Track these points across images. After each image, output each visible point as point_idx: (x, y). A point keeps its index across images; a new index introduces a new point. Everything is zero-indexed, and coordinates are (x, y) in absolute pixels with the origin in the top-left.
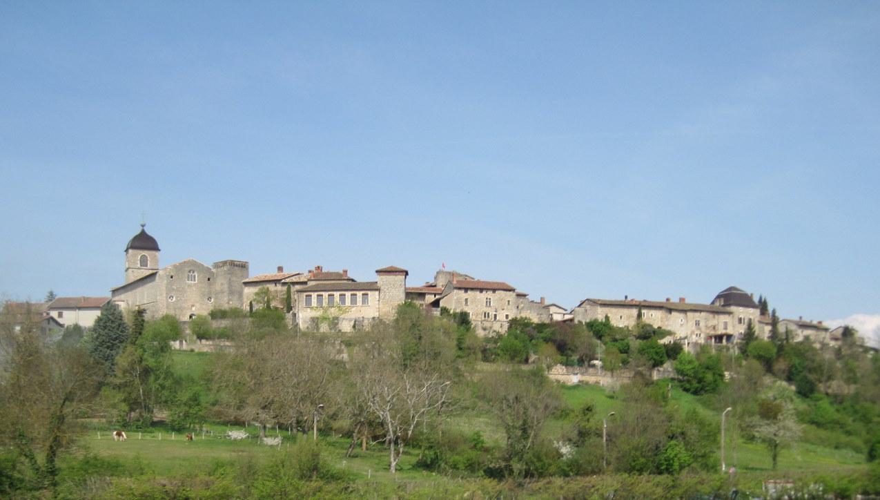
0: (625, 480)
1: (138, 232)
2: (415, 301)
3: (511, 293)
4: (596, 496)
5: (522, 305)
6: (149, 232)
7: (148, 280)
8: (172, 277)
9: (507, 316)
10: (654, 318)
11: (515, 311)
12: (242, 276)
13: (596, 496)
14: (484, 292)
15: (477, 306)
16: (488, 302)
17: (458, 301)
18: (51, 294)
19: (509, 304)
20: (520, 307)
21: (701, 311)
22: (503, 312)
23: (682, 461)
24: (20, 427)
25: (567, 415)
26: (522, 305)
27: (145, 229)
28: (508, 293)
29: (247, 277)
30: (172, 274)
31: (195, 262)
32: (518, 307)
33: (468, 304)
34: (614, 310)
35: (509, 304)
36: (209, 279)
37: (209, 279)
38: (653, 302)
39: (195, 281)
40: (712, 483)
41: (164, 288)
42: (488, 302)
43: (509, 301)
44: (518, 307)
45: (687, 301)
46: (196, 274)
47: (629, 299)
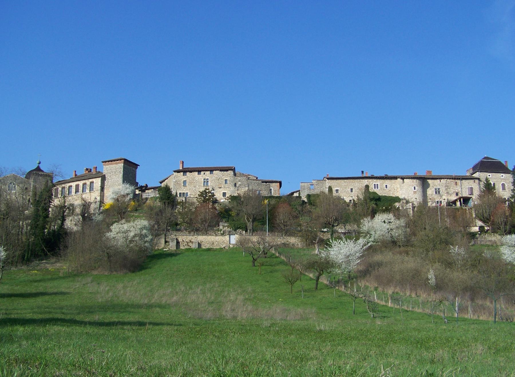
0: (502, 245)
2: (477, 221)
4: (513, 256)
5: (240, 183)
9: (224, 194)
11: (232, 188)
13: (513, 256)
14: (202, 173)
15: (195, 187)
16: (206, 181)
17: (177, 183)
19: (226, 183)
20: (237, 186)
21: (227, 170)
22: (220, 190)
23: (201, 287)
25: (382, 265)
26: (240, 183)
27: (40, 165)
31: (429, 187)
33: (187, 185)
35: (226, 183)
42: (206, 181)
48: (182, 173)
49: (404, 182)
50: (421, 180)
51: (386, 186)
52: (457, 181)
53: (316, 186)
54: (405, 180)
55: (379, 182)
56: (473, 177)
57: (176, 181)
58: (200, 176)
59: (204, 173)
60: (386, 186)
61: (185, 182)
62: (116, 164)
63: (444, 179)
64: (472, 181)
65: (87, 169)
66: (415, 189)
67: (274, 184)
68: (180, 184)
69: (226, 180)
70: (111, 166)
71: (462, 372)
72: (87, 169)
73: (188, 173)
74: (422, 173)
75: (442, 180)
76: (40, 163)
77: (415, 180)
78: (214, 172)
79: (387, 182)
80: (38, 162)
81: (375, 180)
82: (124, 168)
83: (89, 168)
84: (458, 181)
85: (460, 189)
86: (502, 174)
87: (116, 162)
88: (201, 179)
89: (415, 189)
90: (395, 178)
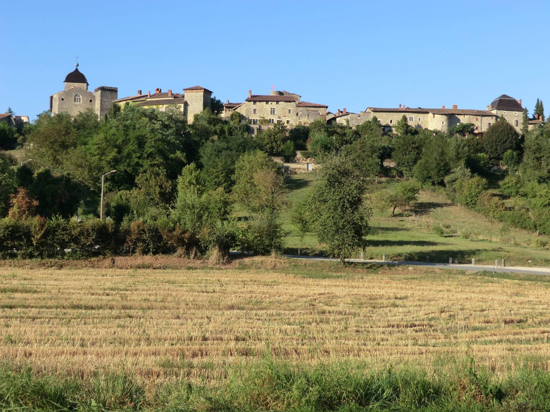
1: (72, 70)
3: (292, 103)
5: (301, 113)
6: (81, 70)
7: (396, 110)
8: (63, 99)
10: (414, 121)
11: (295, 117)
12: (112, 98)
14: (270, 103)
18: (37, 115)
19: (289, 112)
20: (299, 115)
24: (285, 207)
26: (301, 113)
27: (78, 67)
28: (289, 103)
29: (117, 99)
30: (63, 97)
32: (297, 114)
33: (257, 113)
34: (407, 114)
35: (289, 112)
36: (91, 101)
37: (91, 101)
38: (385, 109)
39: (80, 102)
40: (255, 288)
41: (57, 107)
42: (273, 111)
43: (289, 110)
44: (297, 114)
45: (459, 108)
46: (81, 97)
47: (402, 107)
48: (252, 103)
49: (434, 117)
50: (449, 116)
51: (420, 119)
52: (478, 117)
53: (363, 117)
54: (436, 115)
55: (413, 115)
56: (491, 113)
57: (248, 109)
58: (267, 105)
59: (271, 104)
60: (420, 119)
61: (255, 110)
62: (196, 92)
63: (467, 115)
64: (490, 118)
65: (158, 90)
66: (443, 123)
67: (322, 109)
68: (251, 112)
69: (289, 110)
70: (192, 94)
71: (399, 353)
72: (158, 90)
73: (257, 103)
74: (449, 107)
75: (466, 116)
76: (78, 65)
77: (444, 116)
78: (280, 103)
79: (421, 116)
80: (76, 65)
81: (411, 114)
82: (204, 96)
83: (159, 88)
84: (479, 118)
85: (480, 124)
86: (515, 112)
87: (196, 90)
88: (269, 108)
89: (443, 123)
90: (427, 112)
